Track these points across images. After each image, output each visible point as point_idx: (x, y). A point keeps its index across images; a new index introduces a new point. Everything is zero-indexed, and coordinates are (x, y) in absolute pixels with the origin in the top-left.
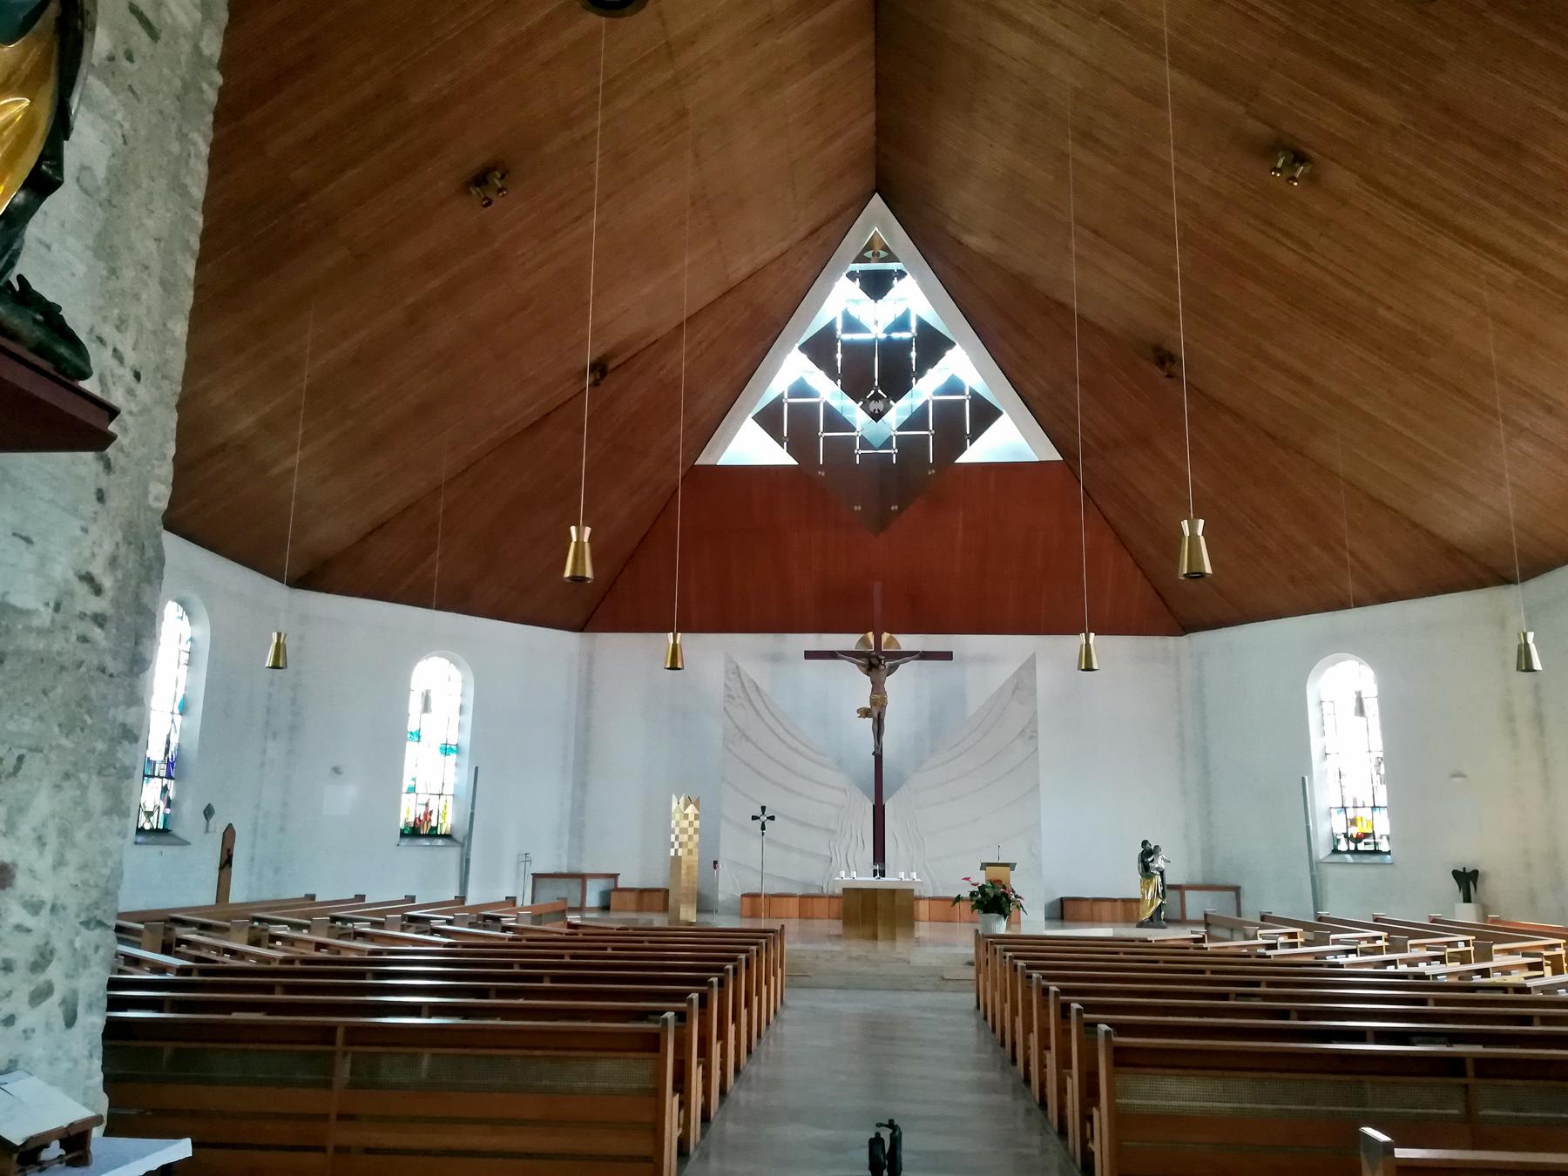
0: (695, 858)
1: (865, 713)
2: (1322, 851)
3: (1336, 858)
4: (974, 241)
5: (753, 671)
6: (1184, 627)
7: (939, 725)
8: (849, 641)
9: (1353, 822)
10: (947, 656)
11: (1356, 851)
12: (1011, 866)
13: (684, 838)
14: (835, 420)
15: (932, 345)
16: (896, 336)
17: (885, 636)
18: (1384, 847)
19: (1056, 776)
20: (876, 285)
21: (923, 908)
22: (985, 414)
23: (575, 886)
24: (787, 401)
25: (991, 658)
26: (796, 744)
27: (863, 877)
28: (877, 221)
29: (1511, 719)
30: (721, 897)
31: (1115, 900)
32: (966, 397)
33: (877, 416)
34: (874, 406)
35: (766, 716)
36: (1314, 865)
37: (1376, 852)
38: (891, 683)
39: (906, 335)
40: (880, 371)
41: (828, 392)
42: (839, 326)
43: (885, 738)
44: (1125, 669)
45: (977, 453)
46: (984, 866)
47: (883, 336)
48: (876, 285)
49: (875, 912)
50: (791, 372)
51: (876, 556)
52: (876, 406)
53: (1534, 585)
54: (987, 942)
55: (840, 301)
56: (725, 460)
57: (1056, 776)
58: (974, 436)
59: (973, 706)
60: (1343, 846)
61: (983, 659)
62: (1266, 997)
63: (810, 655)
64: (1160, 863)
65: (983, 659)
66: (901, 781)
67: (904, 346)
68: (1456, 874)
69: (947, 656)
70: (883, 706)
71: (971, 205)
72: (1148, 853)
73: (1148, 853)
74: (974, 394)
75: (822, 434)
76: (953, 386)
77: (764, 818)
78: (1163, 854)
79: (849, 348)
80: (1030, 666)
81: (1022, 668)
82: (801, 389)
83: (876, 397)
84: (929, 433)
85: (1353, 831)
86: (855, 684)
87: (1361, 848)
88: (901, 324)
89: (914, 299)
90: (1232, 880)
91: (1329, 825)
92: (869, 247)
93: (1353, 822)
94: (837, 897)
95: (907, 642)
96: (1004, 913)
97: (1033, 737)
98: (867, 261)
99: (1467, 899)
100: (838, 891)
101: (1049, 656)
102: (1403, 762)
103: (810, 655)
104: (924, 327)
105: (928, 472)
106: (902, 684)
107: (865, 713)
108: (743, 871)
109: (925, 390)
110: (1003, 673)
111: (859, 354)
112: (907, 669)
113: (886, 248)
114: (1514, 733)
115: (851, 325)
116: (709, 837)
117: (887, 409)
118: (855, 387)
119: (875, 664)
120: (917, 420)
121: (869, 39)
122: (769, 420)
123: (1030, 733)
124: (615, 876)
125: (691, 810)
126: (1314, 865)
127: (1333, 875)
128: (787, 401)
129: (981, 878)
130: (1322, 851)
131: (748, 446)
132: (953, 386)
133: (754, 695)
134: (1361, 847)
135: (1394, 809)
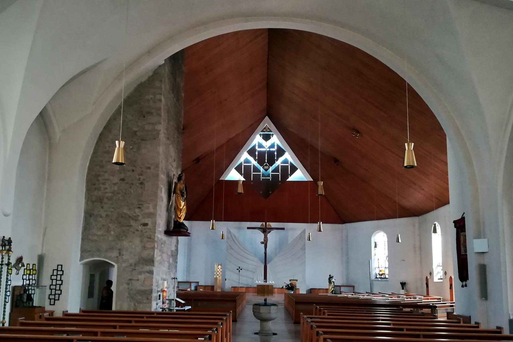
0: (221, 278)
1: (262, 243)
2: (373, 278)
3: (376, 279)
4: (291, 130)
5: (234, 231)
6: (343, 222)
7: (281, 245)
8: (259, 224)
9: (381, 271)
10: (283, 229)
11: (381, 278)
12: (297, 280)
13: (218, 273)
14: (256, 169)
15: (281, 152)
16: (271, 149)
17: (267, 223)
18: (387, 277)
19: (309, 258)
20: (267, 138)
21: (276, 290)
22: (294, 169)
23: (188, 285)
24: (244, 164)
25: (295, 229)
26: (241, 248)
27: (261, 282)
28: (267, 123)
29: (415, 248)
30: (226, 288)
31: (323, 289)
32: (289, 165)
33: (266, 170)
34: (266, 167)
35: (238, 244)
36: (371, 282)
37: (385, 278)
38: (269, 235)
39: (274, 149)
40: (267, 158)
41: (254, 162)
42: (257, 147)
43: (267, 249)
44: (328, 231)
45: (292, 178)
46: (290, 280)
47: (268, 149)
48: (267, 138)
49: (264, 290)
50: (244, 156)
51: (267, 202)
52: (266, 167)
53: (421, 217)
54: (287, 296)
55: (257, 140)
56: (227, 178)
57: (309, 258)
58: (291, 175)
59: (290, 241)
60: (378, 277)
61: (293, 229)
62: (382, 320)
63: (248, 228)
64: (333, 280)
65: (293, 229)
66: (271, 259)
67: (274, 152)
68: (401, 283)
69: (283, 229)
70: (267, 241)
71: (290, 117)
72: (331, 278)
73: (331, 278)
74: (291, 163)
75: (252, 173)
76: (286, 161)
77: (239, 269)
78: (334, 278)
79: (260, 152)
80: (304, 232)
81: (302, 232)
82: (247, 161)
83: (266, 165)
84: (279, 174)
85: (381, 273)
86: (261, 236)
87: (382, 277)
88: (272, 146)
89: (276, 140)
90: (352, 284)
91: (375, 271)
92: (265, 128)
93: (381, 271)
94: (255, 288)
95: (273, 225)
96: (292, 290)
97: (304, 249)
98: (264, 132)
99: (403, 289)
100: (255, 286)
101: (310, 228)
102: (391, 257)
103: (248, 228)
104: (278, 147)
105: (279, 183)
106: (272, 236)
107: (262, 243)
108: (231, 281)
109: (279, 162)
110: (299, 232)
111: (262, 154)
112: (273, 232)
113: (269, 129)
114: (415, 251)
115: (260, 146)
116: (223, 273)
117: (269, 168)
118: (261, 161)
119: (265, 230)
120: (276, 170)
121: (266, 90)
122: (238, 169)
123: (303, 248)
124: (198, 282)
125: (220, 267)
126: (371, 282)
127: (375, 283)
128: (244, 164)
129: (289, 283)
130: (373, 278)
131: (233, 175)
132: (286, 161)
133: (234, 239)
134: (382, 277)
135: (389, 268)
